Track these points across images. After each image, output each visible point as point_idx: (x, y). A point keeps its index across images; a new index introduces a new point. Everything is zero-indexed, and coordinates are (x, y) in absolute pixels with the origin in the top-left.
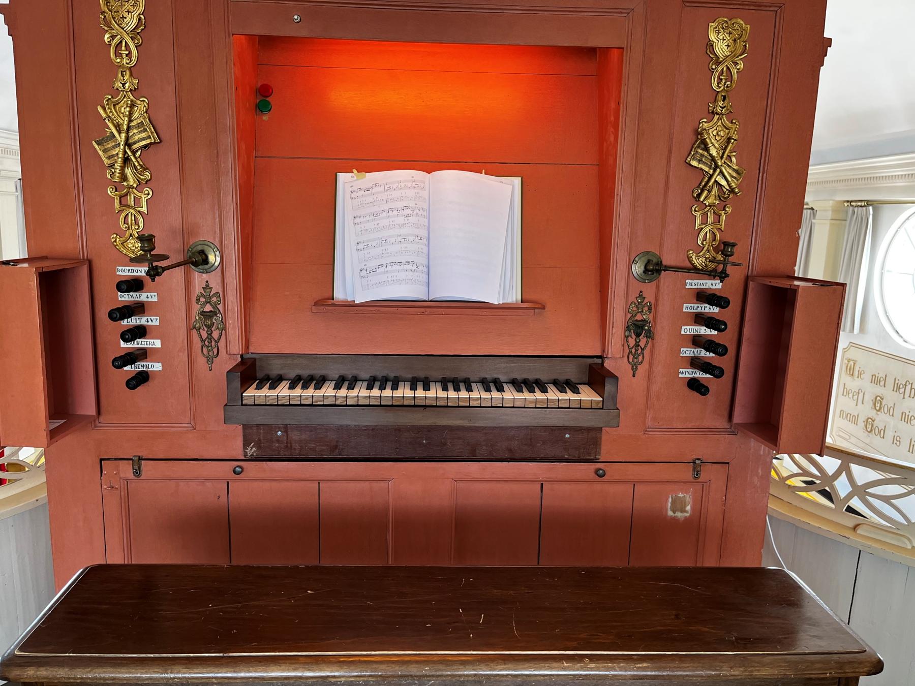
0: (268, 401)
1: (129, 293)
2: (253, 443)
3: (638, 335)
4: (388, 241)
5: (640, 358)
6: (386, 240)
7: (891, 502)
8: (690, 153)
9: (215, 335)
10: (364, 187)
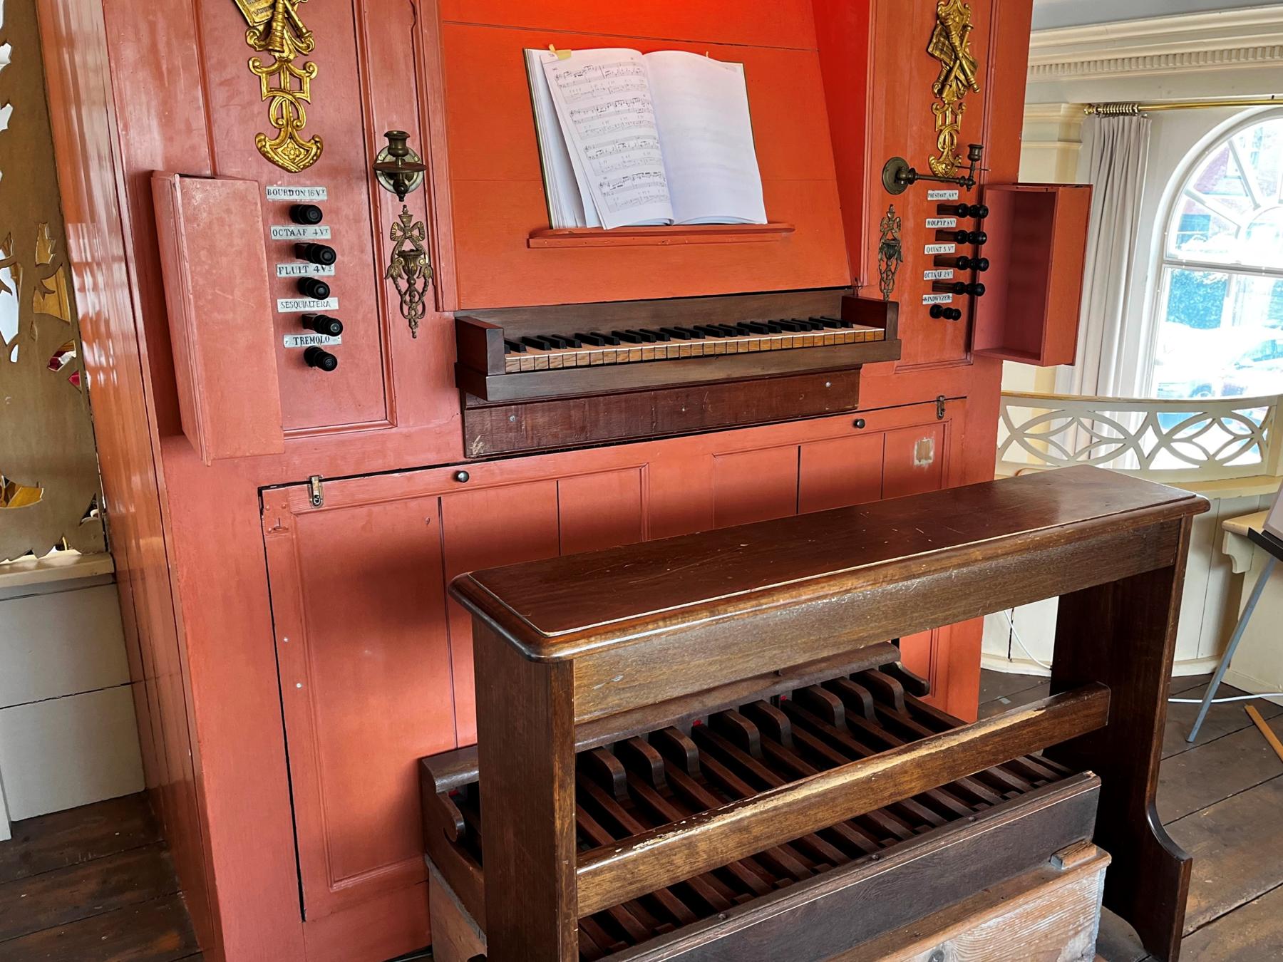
0: (538, 366)
1: (286, 228)
2: (479, 437)
4: (626, 144)
6: (623, 144)
7: (1050, 440)
8: (931, 41)
9: (419, 285)
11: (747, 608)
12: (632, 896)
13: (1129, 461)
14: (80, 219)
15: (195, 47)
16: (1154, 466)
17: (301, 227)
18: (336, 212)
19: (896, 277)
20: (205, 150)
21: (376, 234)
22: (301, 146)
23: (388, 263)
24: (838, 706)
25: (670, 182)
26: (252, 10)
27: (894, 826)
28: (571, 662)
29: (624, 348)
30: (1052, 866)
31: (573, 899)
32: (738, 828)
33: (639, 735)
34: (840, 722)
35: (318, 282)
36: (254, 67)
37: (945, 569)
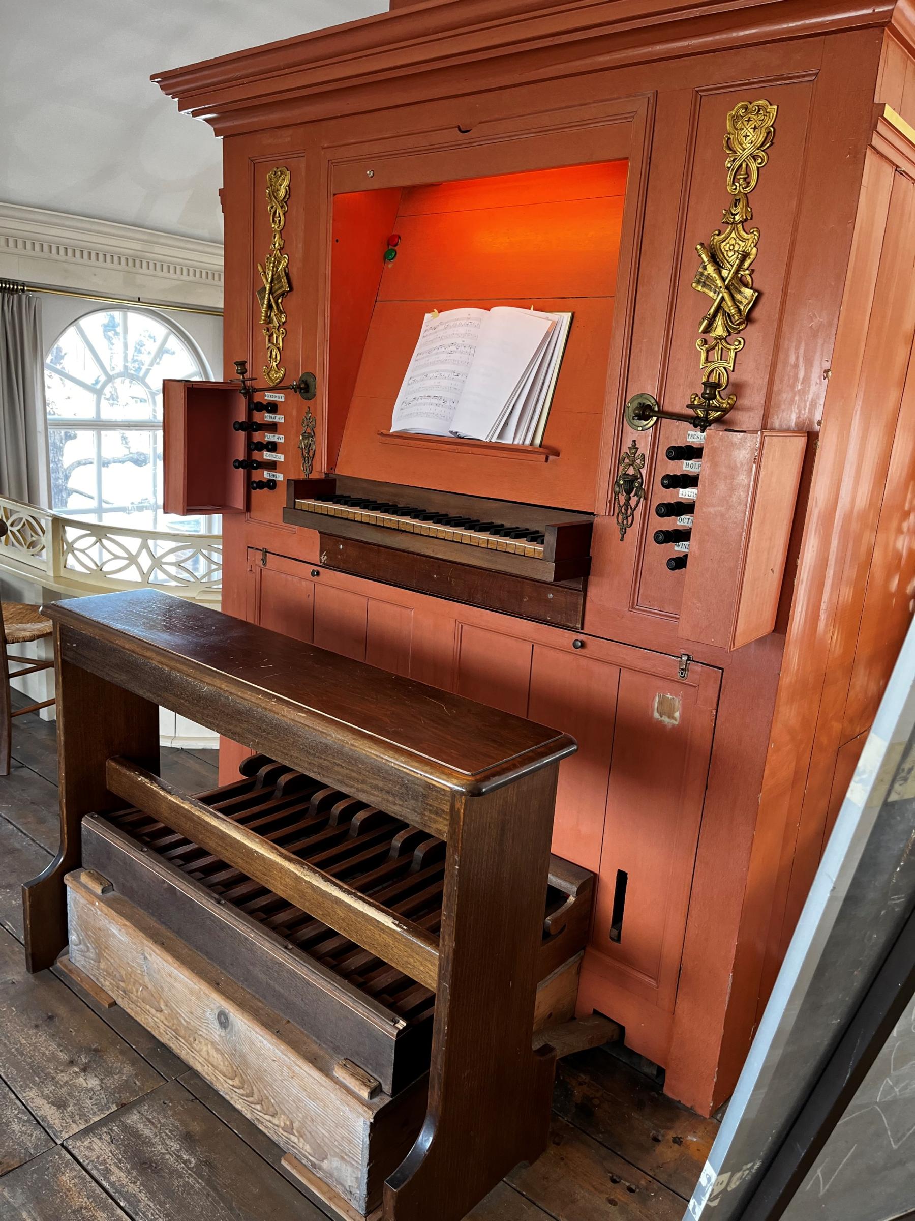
3: (628, 492)
5: (630, 519)
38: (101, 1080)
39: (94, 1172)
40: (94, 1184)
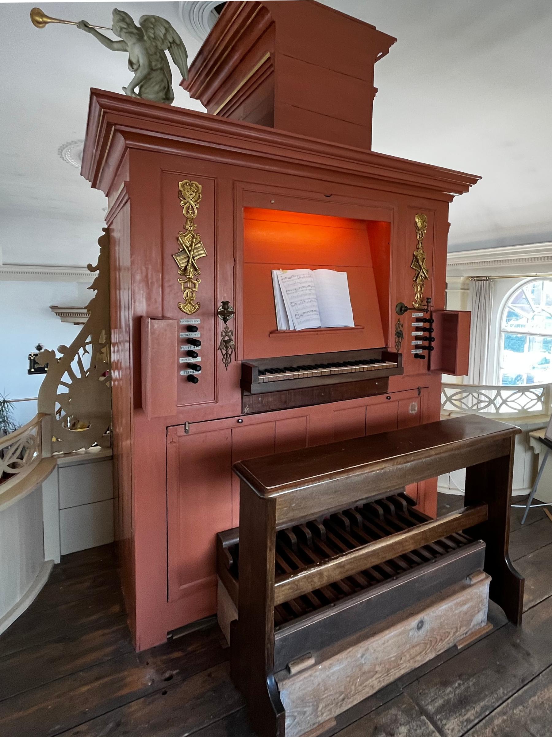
9: (230, 352)
10: (288, 277)
11: (343, 477)
12: (296, 596)
13: (492, 409)
14: (116, 328)
15: (160, 275)
16: (501, 411)
17: (190, 333)
18: (202, 327)
19: (401, 344)
20: (161, 309)
21: (216, 334)
22: (193, 306)
23: (219, 344)
24: (381, 511)
25: (320, 313)
26: (181, 262)
27: (403, 564)
28: (275, 499)
29: (301, 373)
30: (467, 582)
31: (273, 598)
32: (340, 566)
33: (303, 523)
34: (382, 518)
35: (194, 352)
36: (180, 281)
37: (421, 459)
38: (401, 725)
39: (469, 727)
40: (477, 727)
